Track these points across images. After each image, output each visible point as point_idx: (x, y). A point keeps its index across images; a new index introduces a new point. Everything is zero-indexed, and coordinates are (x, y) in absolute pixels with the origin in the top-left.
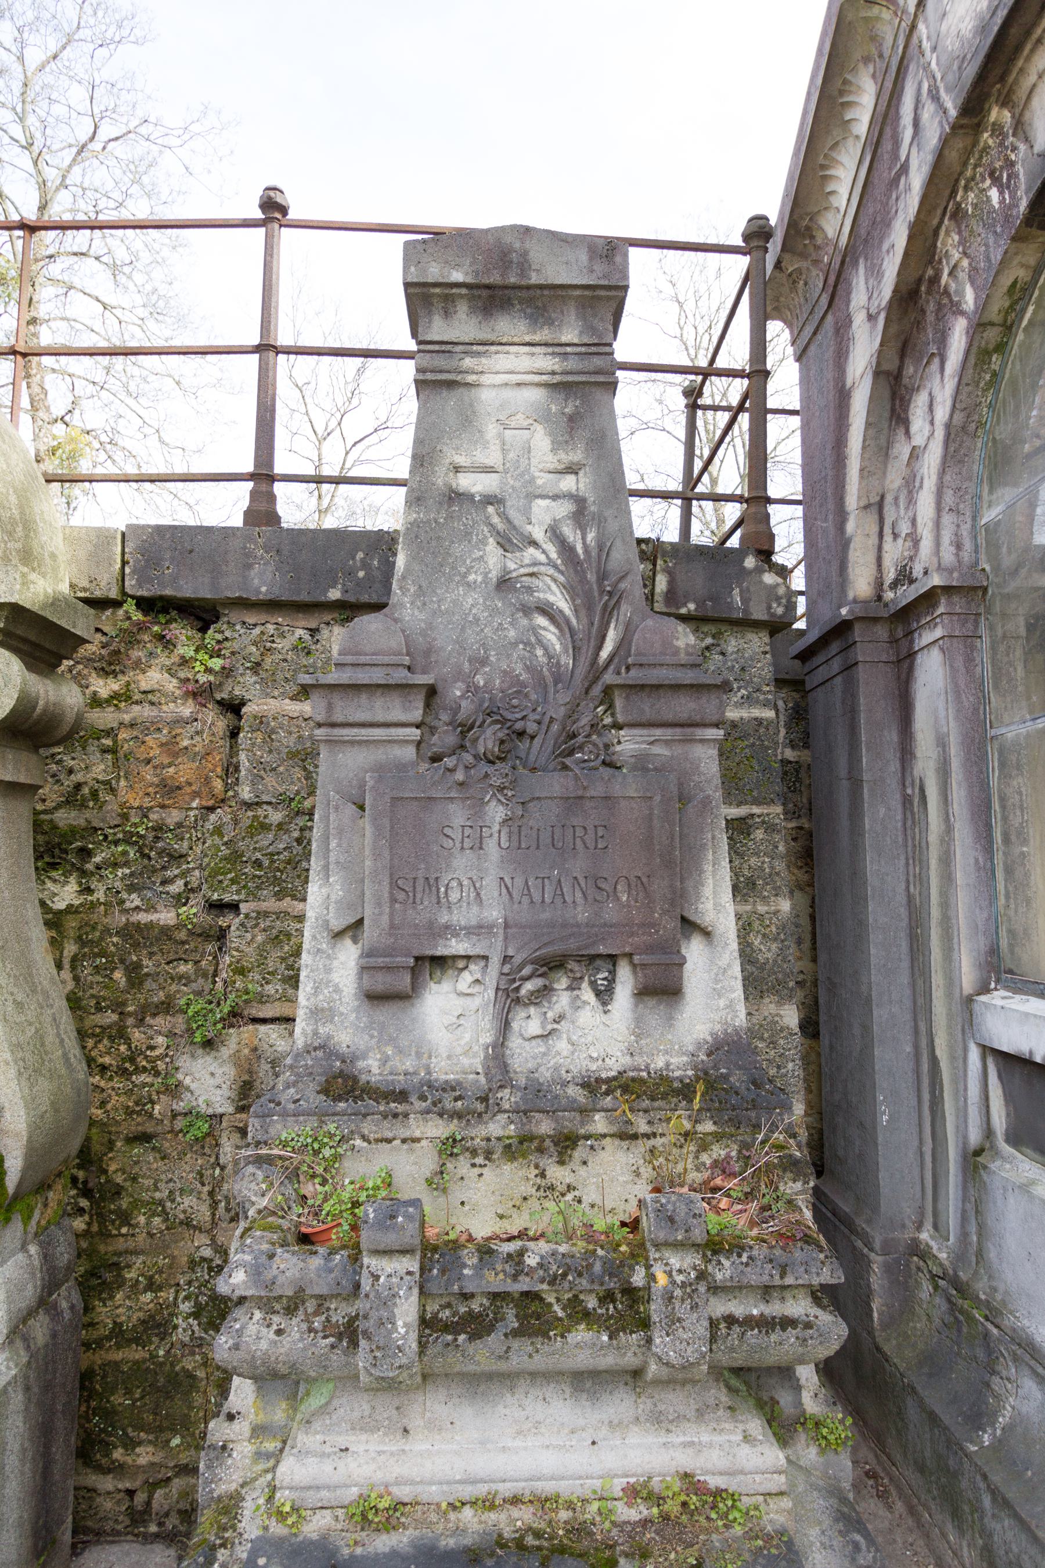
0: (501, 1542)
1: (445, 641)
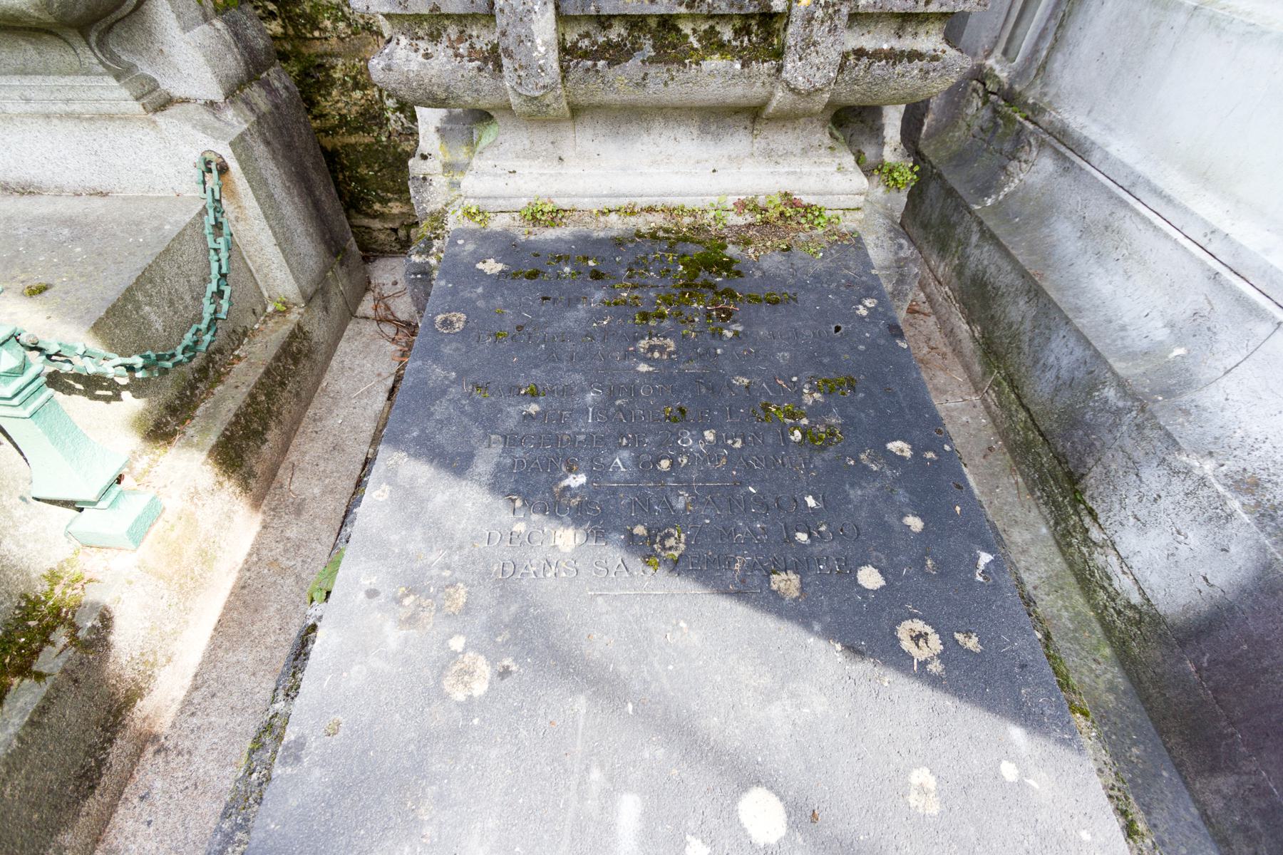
0: (639, 234)
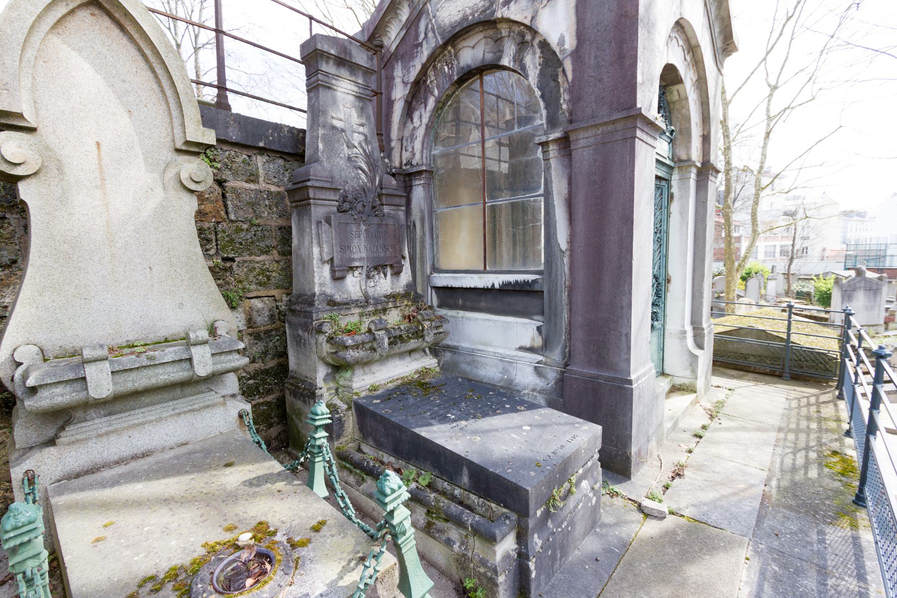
1: (336, 174)
